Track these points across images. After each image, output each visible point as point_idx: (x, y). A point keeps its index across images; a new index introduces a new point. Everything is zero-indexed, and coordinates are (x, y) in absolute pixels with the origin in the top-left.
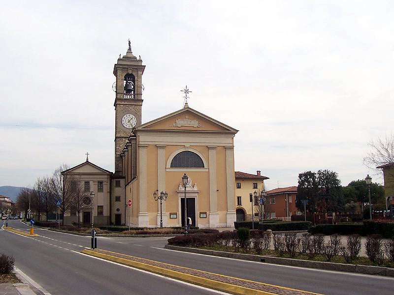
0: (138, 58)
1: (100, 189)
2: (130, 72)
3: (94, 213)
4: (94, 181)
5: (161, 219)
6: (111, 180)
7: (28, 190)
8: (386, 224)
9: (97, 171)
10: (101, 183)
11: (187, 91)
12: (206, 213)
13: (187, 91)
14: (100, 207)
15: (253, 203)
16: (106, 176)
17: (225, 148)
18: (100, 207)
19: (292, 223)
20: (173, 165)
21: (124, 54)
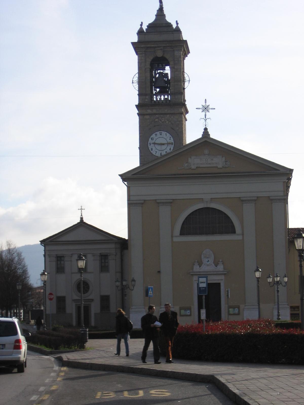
0: (174, 26)
1: (104, 268)
2: (159, 54)
3: (95, 308)
4: (94, 255)
5: (278, 312)
6: (256, 197)
7: (185, 102)
8: (285, 323)
9: (99, 237)
10: (104, 257)
11: (81, 209)
12: (239, 308)
13: (81, 209)
14: (105, 300)
15: (45, 313)
16: (113, 246)
17: (271, 200)
18: (105, 300)
19: (293, 323)
20: (183, 233)
21: (150, 18)
